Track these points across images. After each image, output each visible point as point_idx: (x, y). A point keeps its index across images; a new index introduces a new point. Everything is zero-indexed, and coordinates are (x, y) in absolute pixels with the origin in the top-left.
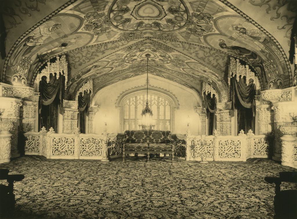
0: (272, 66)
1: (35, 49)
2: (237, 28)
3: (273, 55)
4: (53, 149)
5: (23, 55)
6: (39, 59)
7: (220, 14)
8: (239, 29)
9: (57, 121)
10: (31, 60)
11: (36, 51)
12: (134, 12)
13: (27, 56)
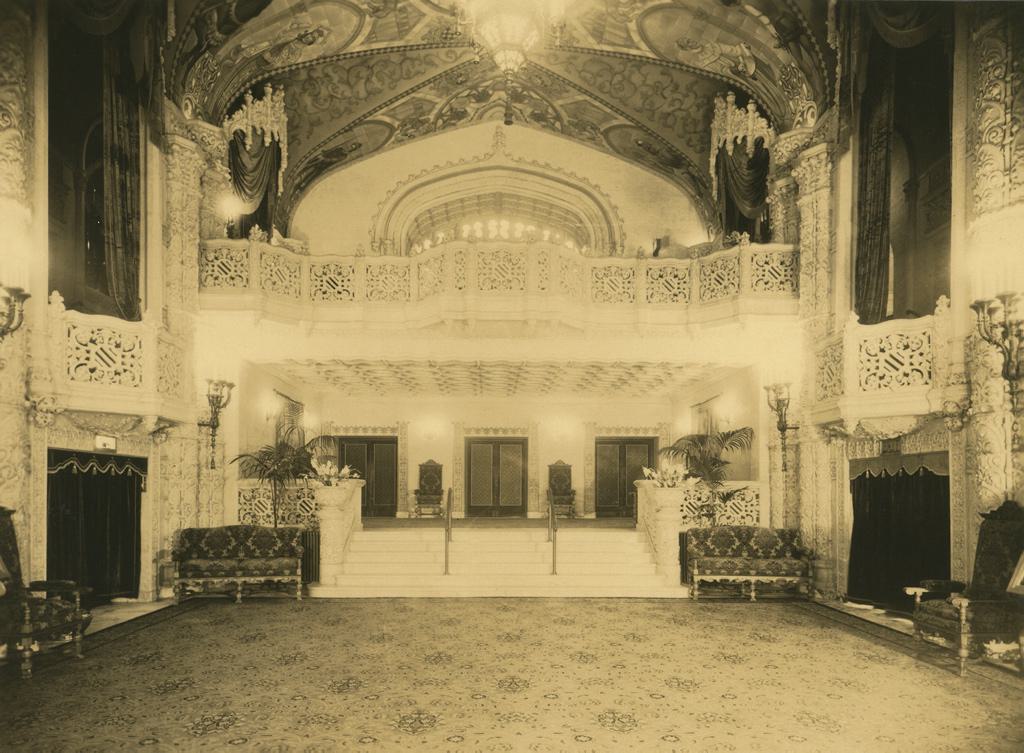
1: (761, 56)
2: (321, 34)
4: (70, 360)
5: (774, 83)
6: (790, 41)
7: (366, 31)
8: (316, 35)
10: (790, 65)
11: (767, 52)
13: (777, 73)
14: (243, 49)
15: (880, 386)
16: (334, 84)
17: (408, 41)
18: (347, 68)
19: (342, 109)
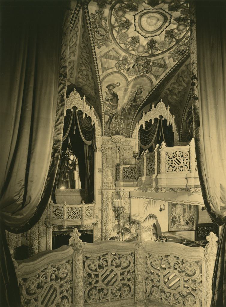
0: (120, 120)
3: (127, 115)
9: (73, 175)
12: (139, 14)
14: (125, 108)
15: (173, 171)
16: (177, 88)
17: (171, 66)
18: (176, 81)
19: (184, 94)
